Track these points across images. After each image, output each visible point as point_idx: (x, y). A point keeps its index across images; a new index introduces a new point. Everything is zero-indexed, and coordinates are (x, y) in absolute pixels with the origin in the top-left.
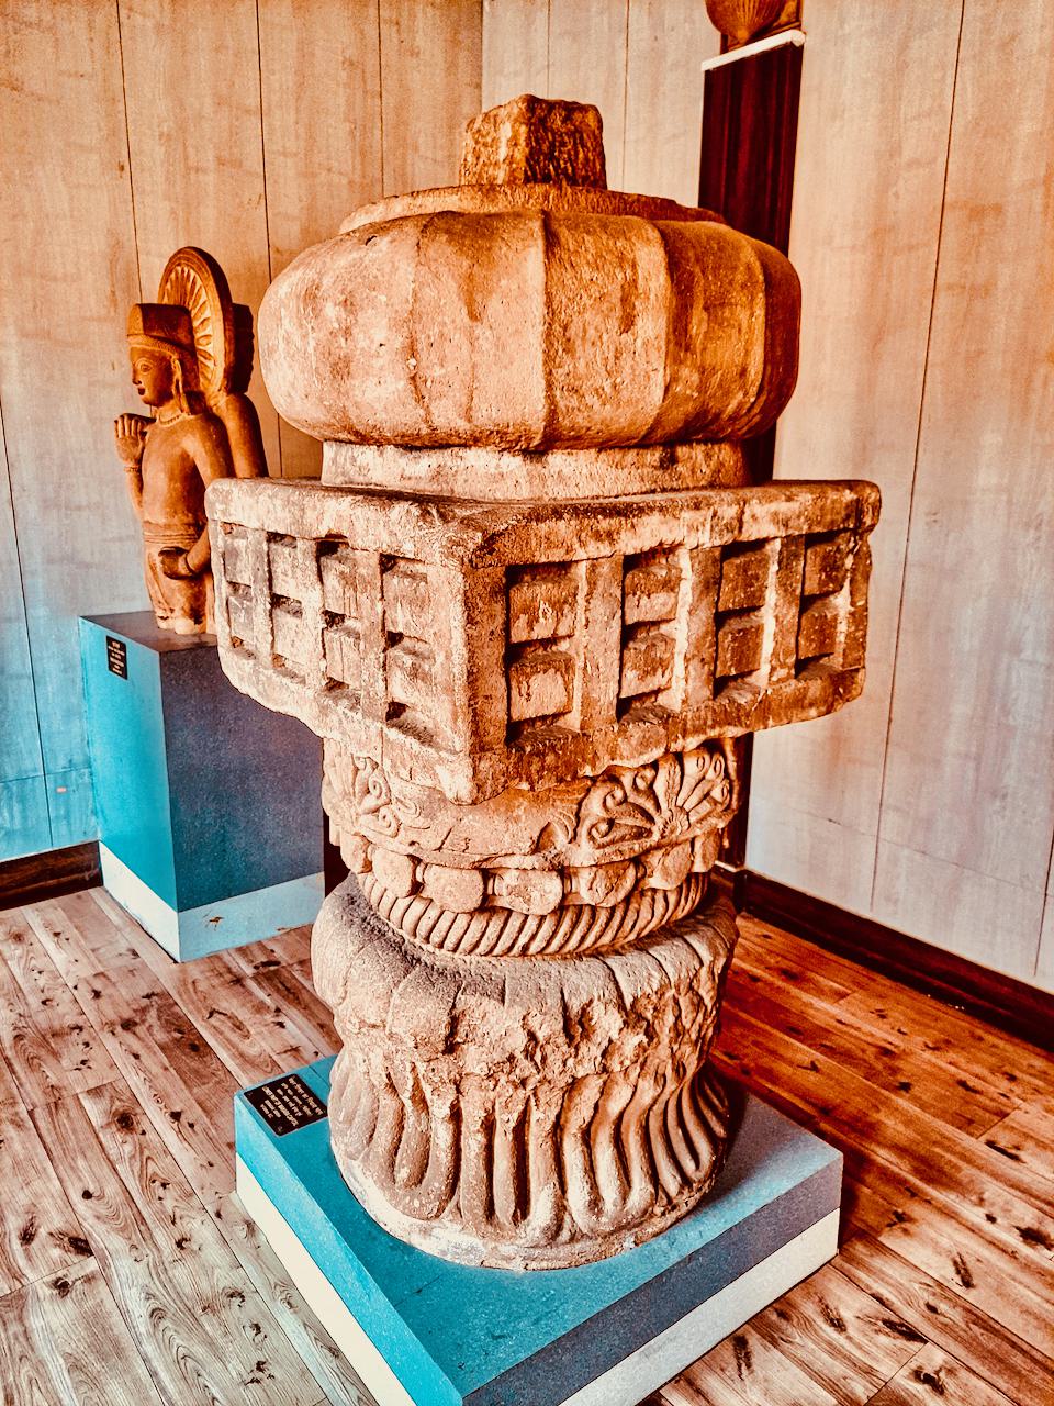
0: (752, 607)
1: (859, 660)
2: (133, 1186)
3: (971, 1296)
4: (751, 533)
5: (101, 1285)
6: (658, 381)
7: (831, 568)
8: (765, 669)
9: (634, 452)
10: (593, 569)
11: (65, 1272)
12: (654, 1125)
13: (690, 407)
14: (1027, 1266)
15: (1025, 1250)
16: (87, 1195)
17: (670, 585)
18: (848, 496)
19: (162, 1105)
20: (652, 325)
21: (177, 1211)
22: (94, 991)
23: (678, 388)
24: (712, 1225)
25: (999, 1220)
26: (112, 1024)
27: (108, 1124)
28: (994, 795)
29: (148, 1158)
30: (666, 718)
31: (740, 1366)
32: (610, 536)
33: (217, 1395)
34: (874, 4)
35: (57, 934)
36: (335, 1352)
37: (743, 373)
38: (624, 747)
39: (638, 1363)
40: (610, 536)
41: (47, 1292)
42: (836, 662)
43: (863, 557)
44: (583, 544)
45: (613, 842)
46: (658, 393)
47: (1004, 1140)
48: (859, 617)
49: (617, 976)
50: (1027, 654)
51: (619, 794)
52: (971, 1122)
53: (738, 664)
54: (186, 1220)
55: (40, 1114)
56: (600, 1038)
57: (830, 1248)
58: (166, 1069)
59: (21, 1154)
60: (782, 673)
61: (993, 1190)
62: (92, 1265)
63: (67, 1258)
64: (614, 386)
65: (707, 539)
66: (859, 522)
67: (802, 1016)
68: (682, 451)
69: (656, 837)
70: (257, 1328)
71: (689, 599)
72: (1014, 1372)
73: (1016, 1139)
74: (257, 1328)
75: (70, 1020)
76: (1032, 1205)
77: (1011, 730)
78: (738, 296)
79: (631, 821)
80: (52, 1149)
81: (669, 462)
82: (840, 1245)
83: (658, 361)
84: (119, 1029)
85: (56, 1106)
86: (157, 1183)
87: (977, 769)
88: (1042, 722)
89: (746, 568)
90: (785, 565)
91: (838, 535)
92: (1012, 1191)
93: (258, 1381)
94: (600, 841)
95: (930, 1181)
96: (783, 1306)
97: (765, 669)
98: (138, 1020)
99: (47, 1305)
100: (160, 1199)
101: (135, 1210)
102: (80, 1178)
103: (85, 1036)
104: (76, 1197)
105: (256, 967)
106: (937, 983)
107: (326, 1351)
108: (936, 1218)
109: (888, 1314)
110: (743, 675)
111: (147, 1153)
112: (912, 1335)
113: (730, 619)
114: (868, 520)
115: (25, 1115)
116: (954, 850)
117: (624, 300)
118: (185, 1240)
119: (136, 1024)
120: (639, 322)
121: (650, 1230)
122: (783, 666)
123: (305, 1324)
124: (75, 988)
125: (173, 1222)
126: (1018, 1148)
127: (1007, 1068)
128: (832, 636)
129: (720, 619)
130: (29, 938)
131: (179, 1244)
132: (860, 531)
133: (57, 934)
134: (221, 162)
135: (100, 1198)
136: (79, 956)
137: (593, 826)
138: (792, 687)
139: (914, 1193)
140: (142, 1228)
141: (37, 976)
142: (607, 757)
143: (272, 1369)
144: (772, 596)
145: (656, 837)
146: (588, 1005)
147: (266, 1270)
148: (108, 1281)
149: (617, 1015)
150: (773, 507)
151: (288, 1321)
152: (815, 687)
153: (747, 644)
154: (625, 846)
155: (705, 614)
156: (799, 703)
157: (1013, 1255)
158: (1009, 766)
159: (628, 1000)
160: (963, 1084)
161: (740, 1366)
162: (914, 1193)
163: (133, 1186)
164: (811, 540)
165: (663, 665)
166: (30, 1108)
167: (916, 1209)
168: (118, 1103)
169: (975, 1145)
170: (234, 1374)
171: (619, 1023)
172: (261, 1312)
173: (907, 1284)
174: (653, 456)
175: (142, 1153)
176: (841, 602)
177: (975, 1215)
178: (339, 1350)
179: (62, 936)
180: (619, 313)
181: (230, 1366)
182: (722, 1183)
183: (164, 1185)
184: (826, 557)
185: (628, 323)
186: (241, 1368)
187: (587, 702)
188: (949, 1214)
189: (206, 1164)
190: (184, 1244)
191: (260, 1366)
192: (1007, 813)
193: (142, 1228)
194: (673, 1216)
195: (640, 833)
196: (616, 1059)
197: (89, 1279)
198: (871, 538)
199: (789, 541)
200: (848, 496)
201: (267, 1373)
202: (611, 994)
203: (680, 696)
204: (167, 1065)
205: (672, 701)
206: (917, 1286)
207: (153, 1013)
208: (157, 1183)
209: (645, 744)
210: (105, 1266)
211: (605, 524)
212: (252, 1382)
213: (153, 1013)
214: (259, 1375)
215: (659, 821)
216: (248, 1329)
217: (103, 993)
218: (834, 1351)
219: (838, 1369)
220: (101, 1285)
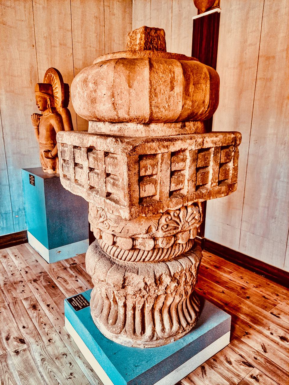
0: (206, 166)
1: (236, 181)
2: (37, 325)
3: (266, 355)
4: (206, 146)
5: (28, 352)
6: (181, 104)
7: (228, 155)
8: (210, 183)
9: (174, 124)
10: (163, 156)
11: (18, 348)
12: (179, 308)
13: (189, 112)
14: (282, 347)
15: (281, 342)
16: (24, 327)
17: (184, 160)
18: (233, 136)
19: (44, 303)
20: (179, 89)
21: (49, 331)
22: (26, 271)
23: (186, 106)
24: (195, 336)
25: (274, 334)
26: (31, 280)
27: (30, 308)
28: (273, 218)
29: (41, 317)
30: (183, 197)
31: (203, 374)
32: (167, 147)
33: (60, 382)
34: (240, 1)
35: (16, 256)
36: (92, 370)
37: (204, 102)
38: (171, 205)
39: (175, 373)
40: (167, 147)
41: (13, 354)
42: (229, 181)
43: (237, 152)
44: (160, 149)
45: (168, 231)
46: (181, 108)
47: (275, 312)
48: (236, 169)
49: (169, 267)
50: (282, 179)
51: (170, 217)
52: (266, 307)
53: (202, 182)
54: (51, 334)
55: (11, 305)
56: (165, 284)
57: (228, 342)
58: (46, 293)
59: (6, 316)
60: (214, 184)
61: (272, 326)
62: (25, 346)
63: (18, 344)
64: (168, 106)
65: (194, 148)
66: (236, 143)
67: (220, 278)
68: (187, 124)
69: (180, 229)
70: (71, 364)
71: (189, 164)
72: (278, 376)
73: (279, 312)
74: (71, 364)
75: (19, 279)
76: (283, 330)
77: (277, 200)
78: (202, 81)
79: (173, 225)
80: (14, 315)
81: (183, 126)
82: (230, 341)
83: (180, 99)
84: (33, 282)
85: (15, 303)
86: (43, 324)
87: (268, 211)
88: (286, 198)
89: (204, 155)
90: (215, 155)
91: (230, 147)
92: (278, 326)
93: (71, 378)
94: (165, 230)
95: (255, 323)
96: (215, 358)
97: (210, 183)
98: (38, 279)
99: (13, 357)
100: (44, 328)
101: (37, 331)
102: (22, 323)
103: (23, 284)
104: (21, 328)
105: (70, 265)
106: (257, 269)
107: (89, 370)
108: (257, 334)
109: (243, 360)
110: (204, 185)
111: (40, 316)
112: (250, 365)
113: (200, 169)
114: (238, 143)
115: (7, 305)
116: (262, 233)
117: (171, 82)
118: (51, 339)
119: (37, 280)
120: (175, 88)
121: (178, 337)
122: (215, 182)
123: (84, 363)
124: (21, 270)
125: (48, 335)
126: (279, 314)
127: (276, 293)
128: (228, 174)
129: (197, 169)
130: (8, 257)
131: (49, 341)
132: (236, 145)
133: (16, 256)
134: (61, 44)
135: (27, 328)
136: (22, 262)
137: (163, 226)
138: (217, 188)
139: (251, 327)
140: (39, 336)
141: (10, 267)
142: (166, 207)
143: (75, 375)
144: (212, 163)
145: (180, 229)
146: (161, 275)
147: (73, 348)
148: (30, 351)
149: (169, 278)
150: (212, 139)
151: (79, 362)
152: (224, 188)
153: (205, 176)
154: (171, 232)
155: (193, 168)
156: (219, 193)
157: (278, 344)
158: (277, 210)
159: (172, 274)
160: (264, 297)
161: (203, 374)
162: (251, 327)
163: (37, 325)
164: (222, 148)
165: (182, 182)
166: (8, 303)
167: (251, 331)
168: (32, 302)
169: (267, 313)
170: (64, 376)
171: (170, 280)
172: (72, 359)
173: (249, 352)
174: (179, 125)
175: (39, 316)
176: (231, 165)
177: (267, 333)
178: (93, 370)
179: (17, 256)
180: (170, 86)
181: (63, 374)
182: (198, 324)
183: (45, 325)
184: (226, 153)
185: (172, 88)
186: (66, 375)
187: (161, 192)
188: (260, 332)
189: (56, 319)
190: (50, 341)
191: (71, 374)
192: (276, 223)
193: (39, 336)
194: (185, 333)
195: (176, 228)
196: (169, 290)
197: (24, 350)
198: (239, 147)
199: (216, 148)
200: (233, 136)
201: (73, 376)
202: (167, 272)
203: (186, 191)
204: (46, 292)
205: (184, 192)
206: (251, 352)
207: (42, 277)
208: (43, 324)
209: (177, 204)
210: (29, 347)
211: (166, 143)
212: (69, 378)
213: (42, 277)
214: (71, 376)
215: (181, 225)
216: (68, 364)
217: (28, 272)
218: (229, 370)
219: (230, 375)
220: (28, 352)
